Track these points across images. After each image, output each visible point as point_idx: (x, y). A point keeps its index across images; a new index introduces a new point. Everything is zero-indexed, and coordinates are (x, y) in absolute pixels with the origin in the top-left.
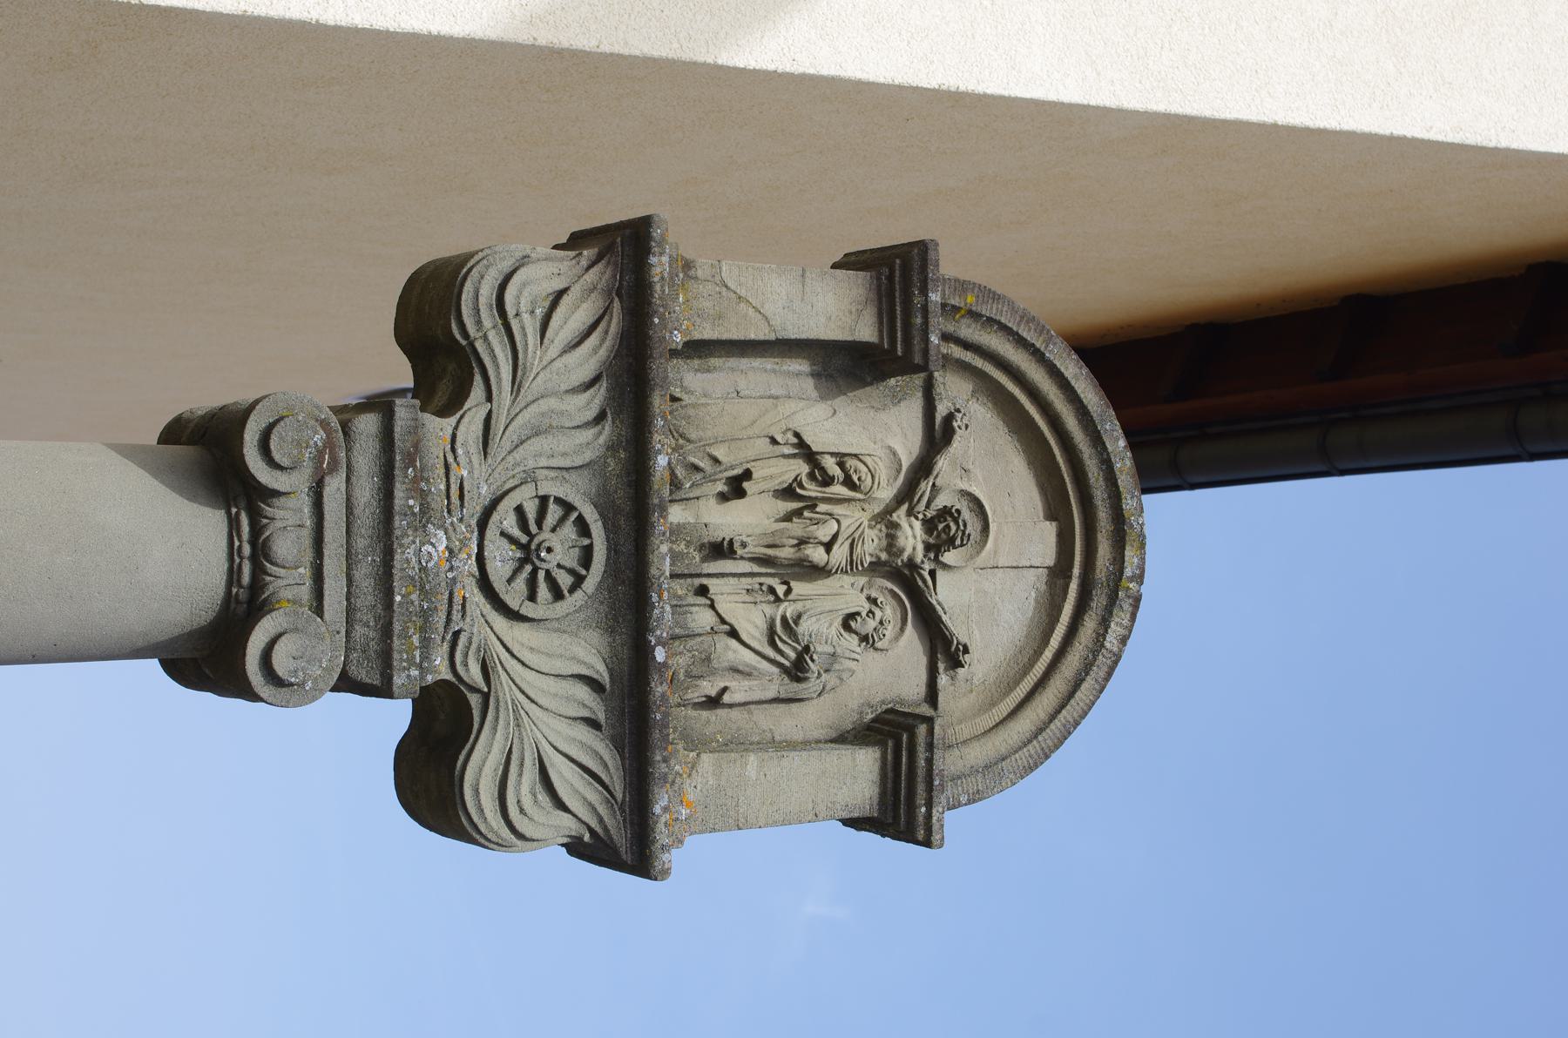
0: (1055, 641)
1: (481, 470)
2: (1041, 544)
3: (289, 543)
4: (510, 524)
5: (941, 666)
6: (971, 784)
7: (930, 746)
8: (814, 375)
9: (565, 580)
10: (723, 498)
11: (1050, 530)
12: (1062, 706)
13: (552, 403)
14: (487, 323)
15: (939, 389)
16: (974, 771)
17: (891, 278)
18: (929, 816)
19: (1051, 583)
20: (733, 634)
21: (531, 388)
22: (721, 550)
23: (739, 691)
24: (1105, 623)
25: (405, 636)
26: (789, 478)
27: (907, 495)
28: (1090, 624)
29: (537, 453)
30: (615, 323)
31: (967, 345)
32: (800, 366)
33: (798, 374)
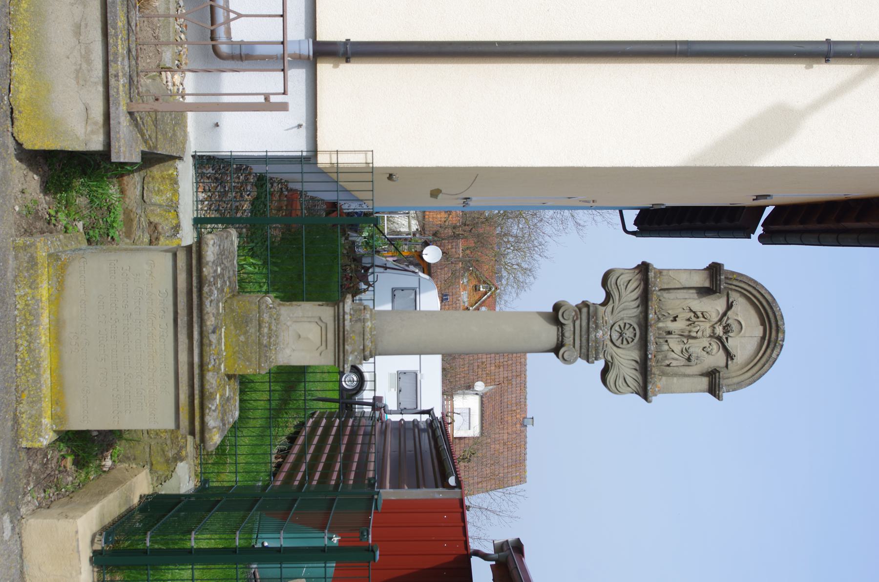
0: (760, 355)
1: (610, 317)
2: (759, 331)
3: (568, 333)
4: (617, 328)
5: (729, 359)
6: (733, 387)
7: (719, 378)
8: (697, 293)
9: (630, 340)
10: (672, 321)
11: (761, 328)
12: (760, 370)
13: (627, 304)
14: (613, 287)
15: (730, 295)
16: (734, 384)
17: (713, 272)
18: (719, 394)
19: (761, 341)
20: (673, 351)
21: (623, 300)
22: (669, 333)
23: (674, 363)
24: (773, 351)
25: (591, 351)
26: (688, 317)
27: (720, 320)
28: (769, 351)
29: (623, 314)
30: (642, 286)
31: (736, 286)
32: (694, 291)
33: (693, 293)
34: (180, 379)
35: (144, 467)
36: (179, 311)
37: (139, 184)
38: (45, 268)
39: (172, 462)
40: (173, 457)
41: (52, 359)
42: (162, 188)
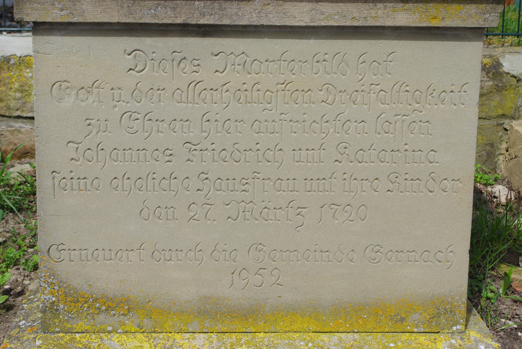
34: (356, 24)
35: (506, 130)
36: (179, 21)
37: (13, 124)
38: (72, 340)
39: (501, 81)
40: (494, 78)
41: (295, 328)
42: (16, 85)
